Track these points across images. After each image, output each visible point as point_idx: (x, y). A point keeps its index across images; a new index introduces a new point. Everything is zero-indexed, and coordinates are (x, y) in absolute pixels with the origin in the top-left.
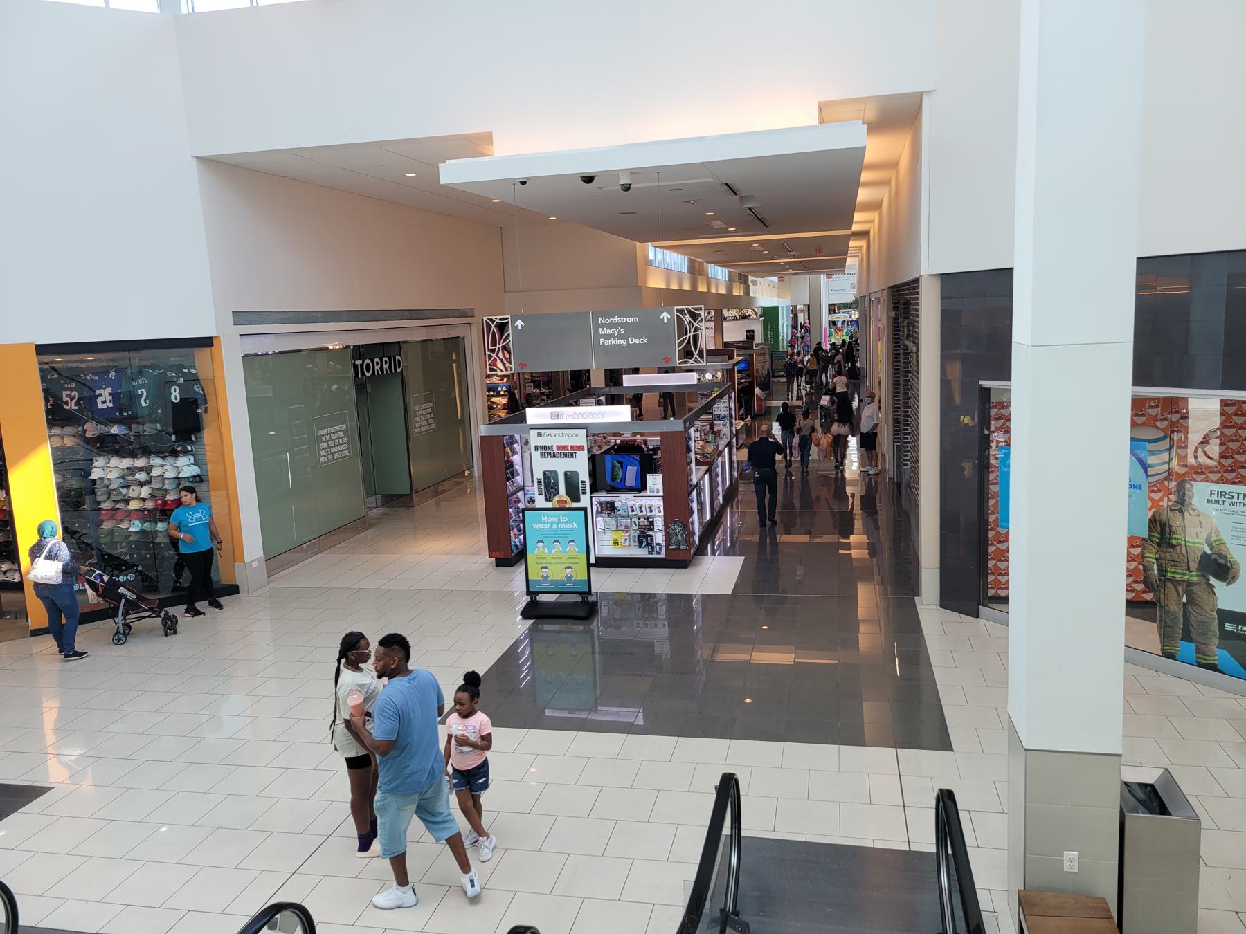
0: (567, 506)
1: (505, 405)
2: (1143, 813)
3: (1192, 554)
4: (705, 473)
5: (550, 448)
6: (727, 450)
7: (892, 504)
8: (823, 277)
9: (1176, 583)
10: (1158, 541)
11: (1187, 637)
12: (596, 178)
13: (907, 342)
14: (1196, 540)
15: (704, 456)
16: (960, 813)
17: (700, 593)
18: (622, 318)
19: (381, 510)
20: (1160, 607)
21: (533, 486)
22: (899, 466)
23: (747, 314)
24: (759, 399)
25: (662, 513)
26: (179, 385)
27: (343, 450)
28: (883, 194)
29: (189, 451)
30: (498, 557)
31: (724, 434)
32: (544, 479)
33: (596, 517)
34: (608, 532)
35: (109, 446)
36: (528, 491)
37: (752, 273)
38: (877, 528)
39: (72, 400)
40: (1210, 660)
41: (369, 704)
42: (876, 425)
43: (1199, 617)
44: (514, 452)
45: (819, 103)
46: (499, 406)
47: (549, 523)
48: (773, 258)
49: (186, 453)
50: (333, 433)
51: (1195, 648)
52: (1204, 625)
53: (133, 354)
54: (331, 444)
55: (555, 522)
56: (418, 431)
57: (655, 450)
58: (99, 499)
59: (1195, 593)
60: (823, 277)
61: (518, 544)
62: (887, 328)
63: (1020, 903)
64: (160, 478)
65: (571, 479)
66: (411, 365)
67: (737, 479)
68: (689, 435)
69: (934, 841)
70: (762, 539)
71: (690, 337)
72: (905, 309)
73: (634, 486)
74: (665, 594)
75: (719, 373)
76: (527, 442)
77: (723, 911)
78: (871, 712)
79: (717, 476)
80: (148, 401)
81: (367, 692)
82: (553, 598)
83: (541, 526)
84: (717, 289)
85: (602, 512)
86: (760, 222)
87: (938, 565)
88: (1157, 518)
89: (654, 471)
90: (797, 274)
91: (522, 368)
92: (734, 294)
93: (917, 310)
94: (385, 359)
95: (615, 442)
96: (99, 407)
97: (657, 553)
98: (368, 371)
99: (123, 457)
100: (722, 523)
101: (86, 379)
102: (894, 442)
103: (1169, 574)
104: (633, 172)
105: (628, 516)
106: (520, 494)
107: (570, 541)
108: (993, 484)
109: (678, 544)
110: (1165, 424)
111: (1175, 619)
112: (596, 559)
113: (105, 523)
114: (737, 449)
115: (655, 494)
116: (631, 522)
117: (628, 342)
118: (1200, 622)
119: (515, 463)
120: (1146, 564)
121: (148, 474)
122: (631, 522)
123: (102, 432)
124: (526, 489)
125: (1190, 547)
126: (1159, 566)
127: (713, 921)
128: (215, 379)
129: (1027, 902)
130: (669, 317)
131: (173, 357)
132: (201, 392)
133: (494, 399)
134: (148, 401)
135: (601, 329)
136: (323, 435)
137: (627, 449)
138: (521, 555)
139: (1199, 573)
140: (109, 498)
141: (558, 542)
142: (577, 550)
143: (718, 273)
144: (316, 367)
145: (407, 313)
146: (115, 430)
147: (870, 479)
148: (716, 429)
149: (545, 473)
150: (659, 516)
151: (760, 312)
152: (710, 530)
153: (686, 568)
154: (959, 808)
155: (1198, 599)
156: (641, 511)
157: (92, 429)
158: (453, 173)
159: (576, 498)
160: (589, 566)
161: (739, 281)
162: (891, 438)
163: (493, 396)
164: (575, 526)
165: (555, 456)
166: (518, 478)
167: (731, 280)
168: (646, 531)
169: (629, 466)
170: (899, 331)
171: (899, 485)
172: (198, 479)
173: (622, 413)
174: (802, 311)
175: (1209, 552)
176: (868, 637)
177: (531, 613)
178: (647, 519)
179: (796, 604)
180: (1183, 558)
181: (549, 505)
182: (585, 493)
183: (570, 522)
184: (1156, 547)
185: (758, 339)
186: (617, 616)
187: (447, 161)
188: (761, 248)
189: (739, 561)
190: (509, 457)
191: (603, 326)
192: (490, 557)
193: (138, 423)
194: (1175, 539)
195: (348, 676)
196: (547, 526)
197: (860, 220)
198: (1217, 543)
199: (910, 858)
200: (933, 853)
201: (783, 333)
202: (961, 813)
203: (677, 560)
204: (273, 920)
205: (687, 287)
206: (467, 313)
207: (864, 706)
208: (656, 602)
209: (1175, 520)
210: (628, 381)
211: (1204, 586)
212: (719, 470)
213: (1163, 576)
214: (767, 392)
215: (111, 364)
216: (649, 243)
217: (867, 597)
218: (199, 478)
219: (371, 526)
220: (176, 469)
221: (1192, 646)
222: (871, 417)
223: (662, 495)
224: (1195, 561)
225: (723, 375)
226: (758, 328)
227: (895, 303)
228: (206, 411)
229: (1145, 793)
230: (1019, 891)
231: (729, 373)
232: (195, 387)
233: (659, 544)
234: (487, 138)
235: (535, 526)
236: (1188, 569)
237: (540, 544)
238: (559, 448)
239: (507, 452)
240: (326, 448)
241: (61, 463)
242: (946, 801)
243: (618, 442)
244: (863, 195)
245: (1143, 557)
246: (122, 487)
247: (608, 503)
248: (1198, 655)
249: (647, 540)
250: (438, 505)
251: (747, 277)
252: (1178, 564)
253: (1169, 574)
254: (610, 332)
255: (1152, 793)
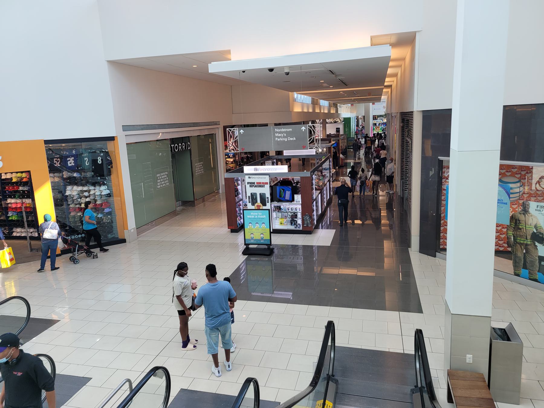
0: (261, 208)
1: (232, 162)
2: (500, 340)
3: (528, 232)
4: (319, 194)
5: (254, 183)
6: (328, 183)
7: (400, 206)
8: (371, 104)
9: (521, 244)
10: (514, 226)
11: (525, 267)
12: (274, 69)
13: (407, 139)
14: (530, 227)
15: (319, 186)
16: (424, 338)
17: (316, 245)
18: (285, 129)
19: (181, 208)
20: (514, 254)
21: (246, 199)
22: (403, 190)
23: (337, 121)
24: (342, 160)
25: (301, 211)
26: (101, 156)
27: (167, 183)
28: (399, 71)
29: (105, 184)
30: (232, 229)
31: (327, 176)
32: (251, 196)
33: (273, 212)
34: (278, 219)
35: (73, 181)
36: (244, 201)
37: (339, 103)
38: (393, 217)
39: (58, 162)
40: (535, 277)
41: (185, 290)
42: (393, 172)
43: (531, 259)
44: (238, 185)
45: (371, 36)
46: (230, 162)
47: (254, 215)
48: (349, 97)
49: (104, 184)
50: (162, 176)
51: (528, 272)
52: (532, 262)
53: (83, 143)
54: (162, 180)
55: (256, 215)
56: (197, 174)
57: (297, 183)
58: (69, 203)
59: (529, 249)
60: (371, 104)
61: (240, 223)
62: (399, 130)
63: (448, 375)
64: (94, 195)
65: (262, 196)
66: (194, 146)
67: (332, 196)
68: (312, 178)
69: (414, 349)
70: (342, 222)
71: (314, 136)
72: (407, 123)
73: (289, 199)
74: (302, 245)
75: (325, 149)
76: (244, 180)
77: (328, 375)
78: (389, 296)
79: (324, 194)
80: (88, 163)
81: (184, 285)
82: (255, 246)
83: (250, 217)
84: (324, 111)
85: (275, 210)
86: (344, 84)
87: (419, 235)
88: (514, 216)
89: (297, 193)
90: (359, 103)
91: (243, 150)
92: (331, 112)
93: (412, 125)
94: (183, 144)
95: (280, 179)
96: (69, 165)
97: (299, 228)
98: (176, 149)
99: (78, 186)
100: (326, 215)
101: (63, 153)
102: (401, 180)
103: (518, 241)
104: (290, 67)
105: (286, 212)
106: (241, 202)
107: (263, 223)
108: (443, 200)
109: (307, 224)
110: (518, 176)
111: (520, 259)
112: (273, 230)
113: (72, 213)
114: (333, 182)
115: (298, 203)
116: (288, 214)
117: (287, 139)
118: (531, 261)
119: (239, 189)
120: (509, 236)
121: (89, 193)
122: (288, 214)
123: (70, 176)
124: (243, 200)
125: (527, 229)
126: (514, 237)
127: (324, 378)
128: (116, 154)
129: (451, 374)
130: (305, 129)
131: (99, 145)
132: (110, 159)
133: (227, 159)
134: (88, 163)
135: (276, 134)
136: (158, 177)
137: (285, 183)
138: (242, 227)
139: (531, 241)
140: (73, 203)
141: (257, 223)
142: (266, 227)
143: (324, 103)
144: (151, 145)
145: (192, 124)
146: (75, 175)
147: (390, 196)
148: (323, 174)
149: (251, 194)
150: (300, 212)
151: (342, 120)
152: (321, 218)
153: (311, 234)
154: (424, 336)
155: (531, 251)
156: (292, 210)
157: (66, 174)
158: (214, 68)
159: (264, 204)
160: (271, 233)
161: (333, 107)
162: (400, 178)
163: (227, 158)
164: (265, 217)
165: (256, 186)
166: (240, 195)
167: (330, 106)
168: (294, 218)
169: (287, 191)
170: (404, 131)
171: (403, 198)
172: (109, 195)
173: (283, 169)
174: (361, 118)
175: (535, 231)
176: (388, 263)
177: (247, 251)
178: (295, 213)
179: (357, 250)
180: (524, 234)
181: (253, 207)
182: (268, 202)
183: (263, 215)
184: (513, 229)
185: (342, 132)
186: (282, 254)
187: (212, 63)
188: (343, 94)
189: (334, 231)
190: (236, 186)
191: (277, 132)
192: (228, 229)
193: (84, 172)
194: (521, 226)
195: (177, 278)
196: (253, 217)
197: (388, 81)
198: (539, 228)
199: (404, 356)
200: (413, 354)
201: (353, 129)
202: (425, 339)
203: (307, 231)
204: (155, 373)
205: (311, 110)
206: (217, 123)
207: (386, 294)
208: (298, 249)
209: (522, 217)
210: (286, 153)
211: (533, 246)
212: (325, 192)
213: (515, 241)
214: (345, 156)
215: (73, 147)
216: (295, 92)
217: (388, 246)
218: (109, 195)
219: (178, 214)
220: (100, 191)
221: (527, 271)
222: (390, 169)
223: (301, 203)
224: (529, 235)
225: (326, 150)
226: (341, 127)
227: (402, 119)
228: (112, 167)
229: (501, 332)
230: (448, 370)
231: (329, 148)
232: (108, 157)
233: (299, 224)
234: (229, 52)
235: (248, 217)
236: (527, 239)
237: (250, 224)
238: (257, 183)
239: (236, 185)
240: (160, 182)
241: (55, 188)
242: (419, 334)
243: (281, 179)
244: (390, 71)
245: (507, 233)
246: (78, 198)
247: (277, 206)
248: (530, 275)
249: (294, 222)
250: (204, 205)
251: (337, 104)
252: (522, 236)
253: (518, 241)
254: (280, 135)
255: (504, 332)
